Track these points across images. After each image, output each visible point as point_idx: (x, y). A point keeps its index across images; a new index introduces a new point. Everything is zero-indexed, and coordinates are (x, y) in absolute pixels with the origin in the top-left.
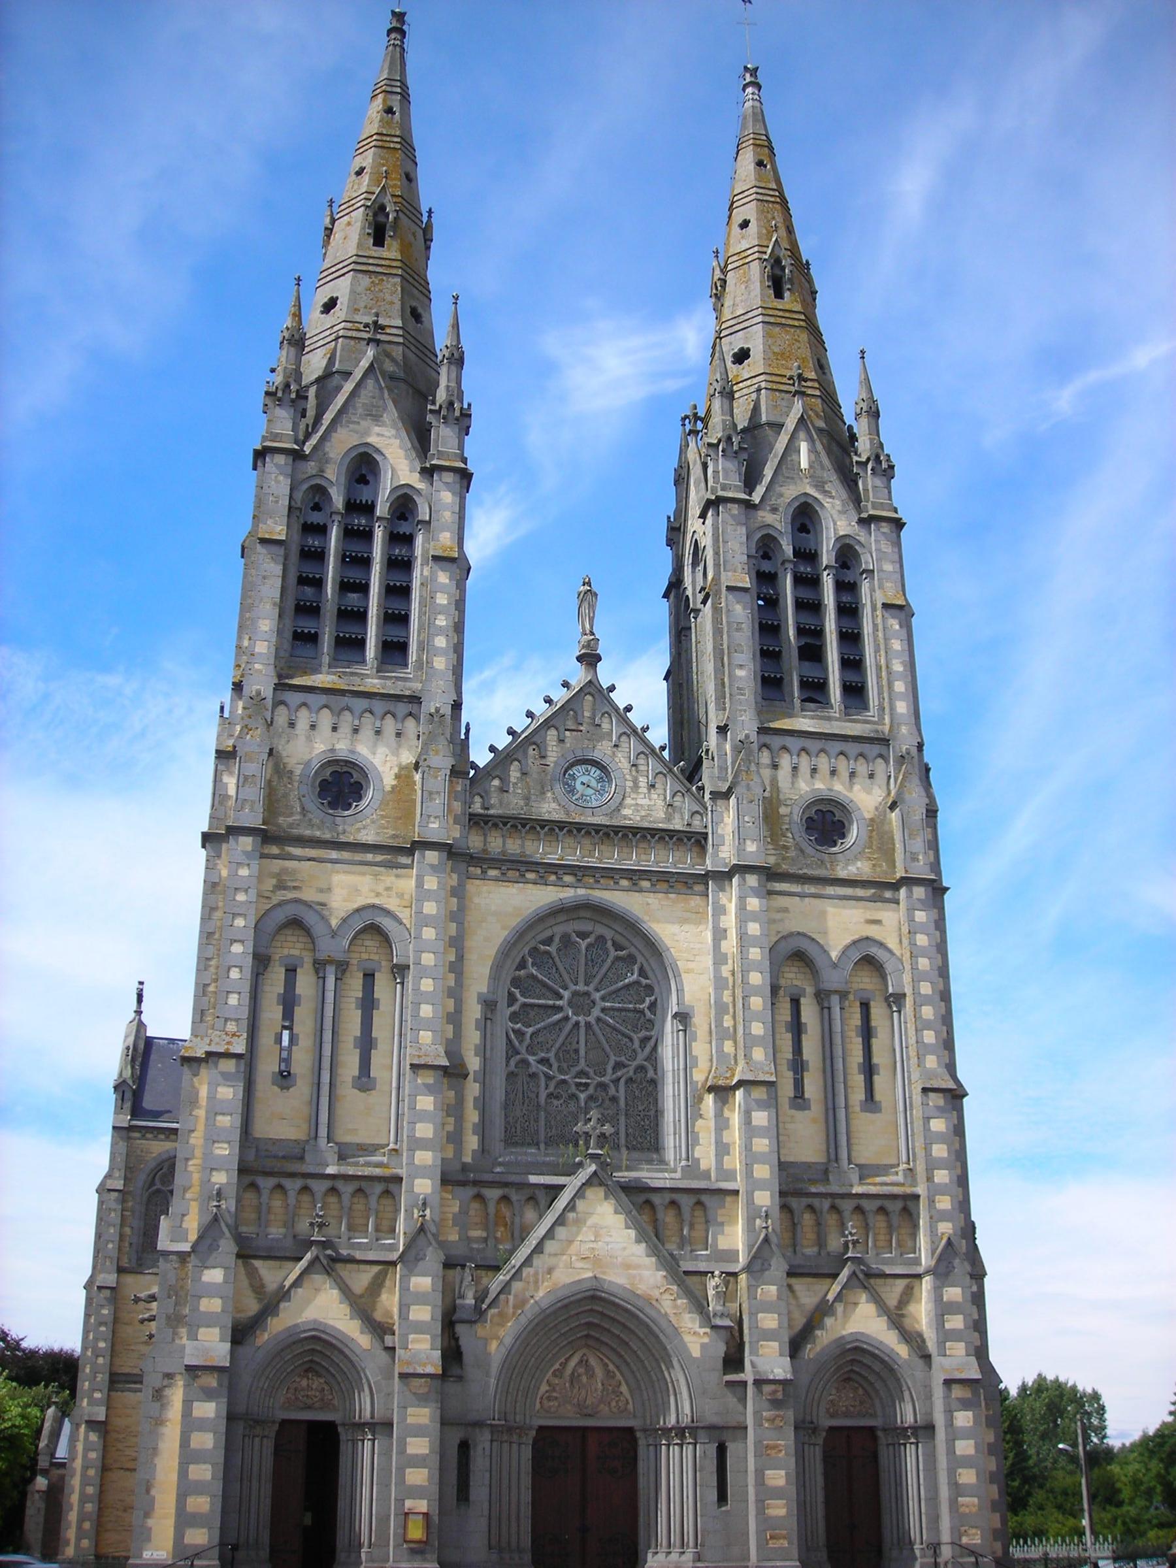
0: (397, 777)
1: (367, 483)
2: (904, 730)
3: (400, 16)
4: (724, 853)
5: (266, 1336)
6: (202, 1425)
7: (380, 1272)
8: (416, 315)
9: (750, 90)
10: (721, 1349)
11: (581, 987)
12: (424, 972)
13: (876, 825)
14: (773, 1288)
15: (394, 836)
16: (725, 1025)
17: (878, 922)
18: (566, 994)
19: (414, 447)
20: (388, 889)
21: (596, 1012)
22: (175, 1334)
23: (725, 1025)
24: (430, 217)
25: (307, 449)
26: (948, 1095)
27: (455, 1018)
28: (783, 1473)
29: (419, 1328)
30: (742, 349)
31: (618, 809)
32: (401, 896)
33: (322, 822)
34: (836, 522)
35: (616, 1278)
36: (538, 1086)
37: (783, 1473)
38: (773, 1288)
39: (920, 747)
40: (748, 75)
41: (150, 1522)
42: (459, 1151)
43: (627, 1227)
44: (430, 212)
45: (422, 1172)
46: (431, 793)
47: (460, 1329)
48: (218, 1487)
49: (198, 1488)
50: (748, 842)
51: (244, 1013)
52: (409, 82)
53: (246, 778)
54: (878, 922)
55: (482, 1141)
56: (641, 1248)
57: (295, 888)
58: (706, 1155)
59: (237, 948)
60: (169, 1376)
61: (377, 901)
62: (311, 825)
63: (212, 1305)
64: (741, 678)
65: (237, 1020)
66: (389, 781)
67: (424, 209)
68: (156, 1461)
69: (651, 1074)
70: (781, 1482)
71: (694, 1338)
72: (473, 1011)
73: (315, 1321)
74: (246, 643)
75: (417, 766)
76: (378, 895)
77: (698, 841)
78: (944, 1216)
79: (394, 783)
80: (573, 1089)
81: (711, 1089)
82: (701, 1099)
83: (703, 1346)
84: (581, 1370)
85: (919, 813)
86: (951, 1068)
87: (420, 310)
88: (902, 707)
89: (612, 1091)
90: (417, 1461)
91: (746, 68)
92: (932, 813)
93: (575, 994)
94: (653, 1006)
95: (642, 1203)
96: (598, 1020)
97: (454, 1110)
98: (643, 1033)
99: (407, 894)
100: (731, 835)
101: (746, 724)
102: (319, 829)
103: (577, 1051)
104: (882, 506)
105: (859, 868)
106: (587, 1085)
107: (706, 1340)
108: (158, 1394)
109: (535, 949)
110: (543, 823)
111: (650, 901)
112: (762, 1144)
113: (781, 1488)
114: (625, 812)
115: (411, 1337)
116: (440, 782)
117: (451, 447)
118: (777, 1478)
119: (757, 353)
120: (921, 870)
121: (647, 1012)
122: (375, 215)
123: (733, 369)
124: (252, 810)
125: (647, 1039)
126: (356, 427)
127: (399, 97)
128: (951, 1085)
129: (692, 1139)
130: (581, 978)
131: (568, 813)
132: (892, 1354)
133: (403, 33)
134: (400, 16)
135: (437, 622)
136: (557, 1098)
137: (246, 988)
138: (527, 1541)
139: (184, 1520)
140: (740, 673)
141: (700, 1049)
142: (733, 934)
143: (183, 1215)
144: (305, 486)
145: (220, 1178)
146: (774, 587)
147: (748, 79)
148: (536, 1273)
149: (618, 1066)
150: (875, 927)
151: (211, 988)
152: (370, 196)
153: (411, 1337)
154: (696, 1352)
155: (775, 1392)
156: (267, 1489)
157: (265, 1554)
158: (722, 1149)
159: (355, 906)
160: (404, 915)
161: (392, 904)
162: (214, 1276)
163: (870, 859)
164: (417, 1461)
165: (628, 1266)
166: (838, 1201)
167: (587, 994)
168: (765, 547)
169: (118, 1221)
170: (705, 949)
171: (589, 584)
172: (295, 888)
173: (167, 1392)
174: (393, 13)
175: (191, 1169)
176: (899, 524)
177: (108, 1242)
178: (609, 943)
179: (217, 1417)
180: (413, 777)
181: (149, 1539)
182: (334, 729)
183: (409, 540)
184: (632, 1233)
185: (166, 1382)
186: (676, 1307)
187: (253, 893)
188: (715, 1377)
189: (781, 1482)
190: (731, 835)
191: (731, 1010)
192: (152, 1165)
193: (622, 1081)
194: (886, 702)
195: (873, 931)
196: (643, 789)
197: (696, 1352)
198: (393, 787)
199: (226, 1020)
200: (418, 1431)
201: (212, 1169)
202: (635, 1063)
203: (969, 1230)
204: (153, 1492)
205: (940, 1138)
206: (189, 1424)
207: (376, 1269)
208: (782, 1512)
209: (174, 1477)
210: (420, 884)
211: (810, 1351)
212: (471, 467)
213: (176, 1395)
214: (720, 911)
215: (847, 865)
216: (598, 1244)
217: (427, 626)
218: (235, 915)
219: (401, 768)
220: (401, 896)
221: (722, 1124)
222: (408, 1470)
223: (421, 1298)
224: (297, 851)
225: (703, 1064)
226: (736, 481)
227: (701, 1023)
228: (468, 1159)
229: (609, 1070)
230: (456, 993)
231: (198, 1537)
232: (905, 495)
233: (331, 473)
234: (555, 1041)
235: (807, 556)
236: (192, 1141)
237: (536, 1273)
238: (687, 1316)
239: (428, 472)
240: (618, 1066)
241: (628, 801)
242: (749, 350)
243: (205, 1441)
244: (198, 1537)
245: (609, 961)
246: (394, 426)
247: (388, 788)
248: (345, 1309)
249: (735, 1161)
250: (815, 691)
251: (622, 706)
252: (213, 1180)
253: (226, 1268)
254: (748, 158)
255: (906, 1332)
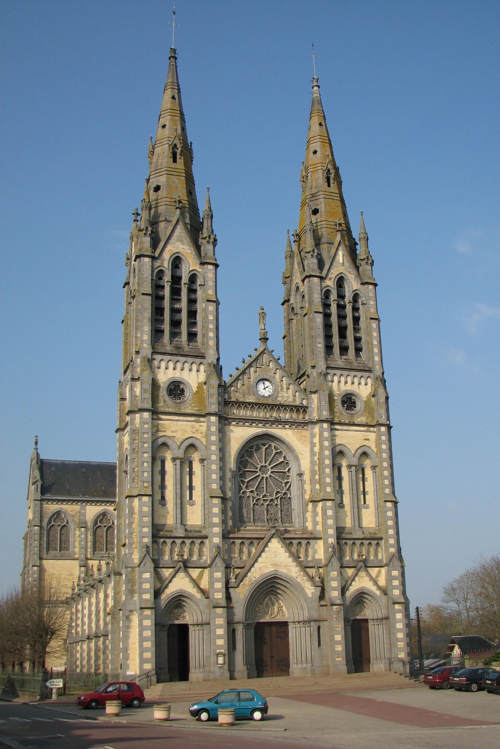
0: (198, 387)
1: (179, 268)
2: (377, 367)
3: (174, 51)
4: (315, 416)
5: (165, 595)
6: (147, 628)
7: (200, 572)
8: (191, 192)
9: (316, 88)
10: (318, 594)
11: (263, 464)
12: (213, 462)
13: (367, 403)
14: (336, 573)
15: (197, 410)
16: (316, 478)
17: (368, 440)
18: (259, 466)
19: (196, 254)
20: (197, 430)
21: (269, 472)
22: (132, 596)
23: (316, 478)
24: (191, 145)
25: (157, 255)
26: (393, 503)
27: (222, 478)
28: (340, 636)
29: (218, 590)
30: (315, 209)
31: (276, 398)
32: (201, 433)
33: (172, 405)
34: (352, 284)
35: (283, 571)
36: (250, 501)
37: (340, 636)
38: (336, 573)
39: (383, 373)
40: (315, 81)
41: (128, 662)
42: (226, 526)
43: (286, 552)
44: (191, 143)
45: (215, 535)
46: (211, 395)
47: (231, 590)
48: (154, 649)
49: (147, 650)
50: (324, 411)
51: (150, 479)
52: (180, 84)
53: (144, 390)
54: (368, 440)
55: (233, 522)
56: (291, 559)
57: (164, 431)
58: (309, 525)
59: (146, 455)
60: (131, 611)
61: (193, 435)
62: (168, 407)
63: (147, 586)
64: (320, 347)
65: (147, 482)
66: (195, 389)
67: (189, 142)
68: (129, 641)
69: (289, 496)
70: (340, 639)
71: (309, 591)
72: (229, 475)
73: (181, 590)
74: (139, 335)
75: (205, 383)
76: (194, 433)
77: (304, 409)
78: (392, 546)
79: (196, 390)
80: (262, 502)
81: (311, 502)
82: (308, 505)
83: (312, 593)
84: (269, 602)
85: (383, 400)
86: (393, 492)
87: (192, 191)
88: (377, 358)
89: (276, 502)
90: (220, 637)
91: (314, 78)
92: (387, 398)
93: (262, 466)
94: (289, 470)
95: (288, 542)
96: (270, 476)
97: (224, 512)
98: (286, 481)
99: (202, 431)
100: (316, 406)
101: (322, 365)
102: (171, 408)
103: (263, 488)
104: (370, 278)
105: (362, 419)
106: (267, 500)
107: (313, 591)
108: (128, 618)
109: (247, 450)
110: (250, 403)
111: (288, 432)
112: (330, 522)
113: (339, 641)
114: (280, 399)
115: (215, 594)
116: (214, 391)
117: (211, 253)
118: (338, 637)
119: (322, 208)
120: (383, 420)
121: (287, 473)
122: (173, 148)
123: (314, 218)
124: (147, 402)
125: (288, 482)
126: (174, 245)
127: (177, 91)
128: (394, 499)
129: (305, 520)
130: (264, 461)
131: (258, 400)
132: (375, 593)
133: (176, 58)
134: (174, 51)
135: (210, 327)
136: (257, 505)
137: (150, 470)
138: (254, 663)
139: (142, 661)
140: (320, 345)
141: (307, 487)
142: (318, 445)
143: (132, 553)
144: (156, 271)
145: (146, 540)
146: (330, 309)
147: (315, 84)
148: (256, 570)
149: (278, 492)
150: (367, 441)
151: (136, 470)
152: (170, 139)
153: (215, 594)
154: (310, 596)
155: (337, 608)
156: (166, 648)
157: (167, 670)
158: (315, 523)
159: (186, 437)
160: (204, 440)
161: (198, 436)
162: (147, 575)
163: (365, 416)
164: (220, 637)
165: (286, 566)
166: (355, 541)
167: (266, 466)
168: (327, 294)
169: (38, 539)
170: (303, 447)
171: (263, 309)
172: (164, 431)
173: (131, 617)
174: (171, 49)
175: (133, 536)
176: (375, 285)
177: (35, 547)
178: (273, 448)
179: (152, 625)
180: (203, 387)
181: (128, 668)
182: (174, 369)
183: (195, 291)
184: (287, 554)
185: (130, 613)
186: (303, 580)
187: (150, 434)
188: (316, 604)
189: (340, 639)
190: (316, 406)
191: (318, 473)
192: (51, 514)
193: (279, 499)
194: (371, 355)
195: (366, 443)
196: (285, 390)
197: (310, 596)
198: (196, 391)
199: (144, 482)
200: (220, 626)
201: (143, 537)
202: (284, 492)
203: (399, 550)
204: (129, 652)
205: (390, 518)
206: (142, 628)
207: (200, 570)
208: (340, 649)
209: (137, 646)
210: (209, 428)
211: (348, 594)
212: (218, 262)
213: (135, 619)
214: (313, 436)
215: (357, 418)
216: (274, 558)
217: (205, 327)
218: (144, 443)
219: (199, 384)
220: (201, 433)
221: (315, 514)
222: (217, 640)
223: (218, 580)
224: (163, 417)
225: (308, 492)
226: (316, 267)
227: (307, 477)
228: (229, 529)
229: (275, 495)
230: (222, 469)
231: (148, 666)
232: (378, 273)
233: (166, 264)
234: (255, 484)
235: (341, 296)
236: (133, 527)
237: (256, 570)
238: (307, 583)
239: (202, 264)
240: (278, 492)
241: (280, 395)
242: (318, 209)
243: (148, 633)
244: (148, 666)
245: (273, 454)
246: (188, 245)
247: (195, 392)
248: (191, 585)
249: (319, 528)
250: (344, 350)
251: (276, 358)
252: (143, 541)
253: (150, 573)
254: (316, 120)
255: (379, 586)
